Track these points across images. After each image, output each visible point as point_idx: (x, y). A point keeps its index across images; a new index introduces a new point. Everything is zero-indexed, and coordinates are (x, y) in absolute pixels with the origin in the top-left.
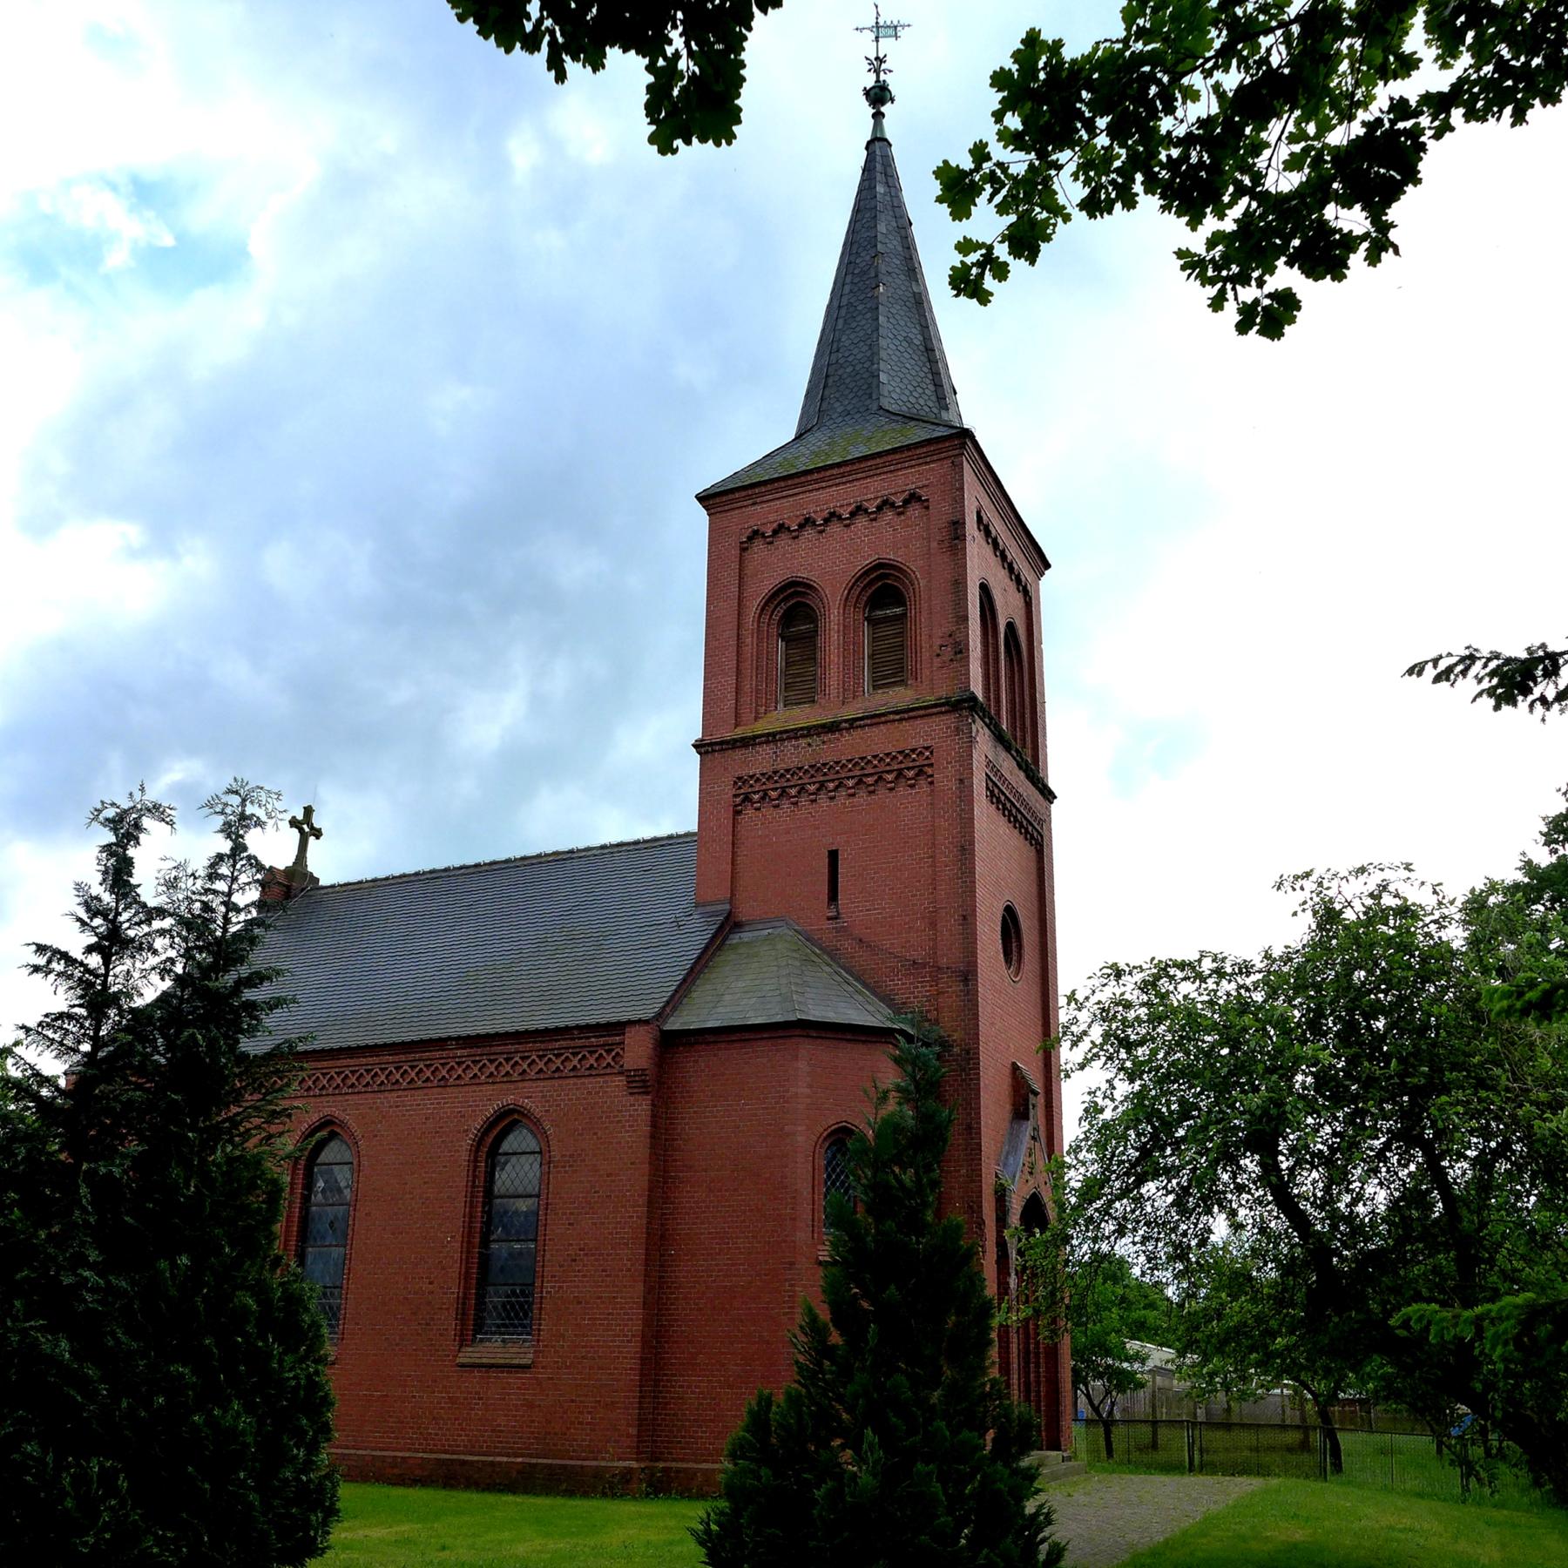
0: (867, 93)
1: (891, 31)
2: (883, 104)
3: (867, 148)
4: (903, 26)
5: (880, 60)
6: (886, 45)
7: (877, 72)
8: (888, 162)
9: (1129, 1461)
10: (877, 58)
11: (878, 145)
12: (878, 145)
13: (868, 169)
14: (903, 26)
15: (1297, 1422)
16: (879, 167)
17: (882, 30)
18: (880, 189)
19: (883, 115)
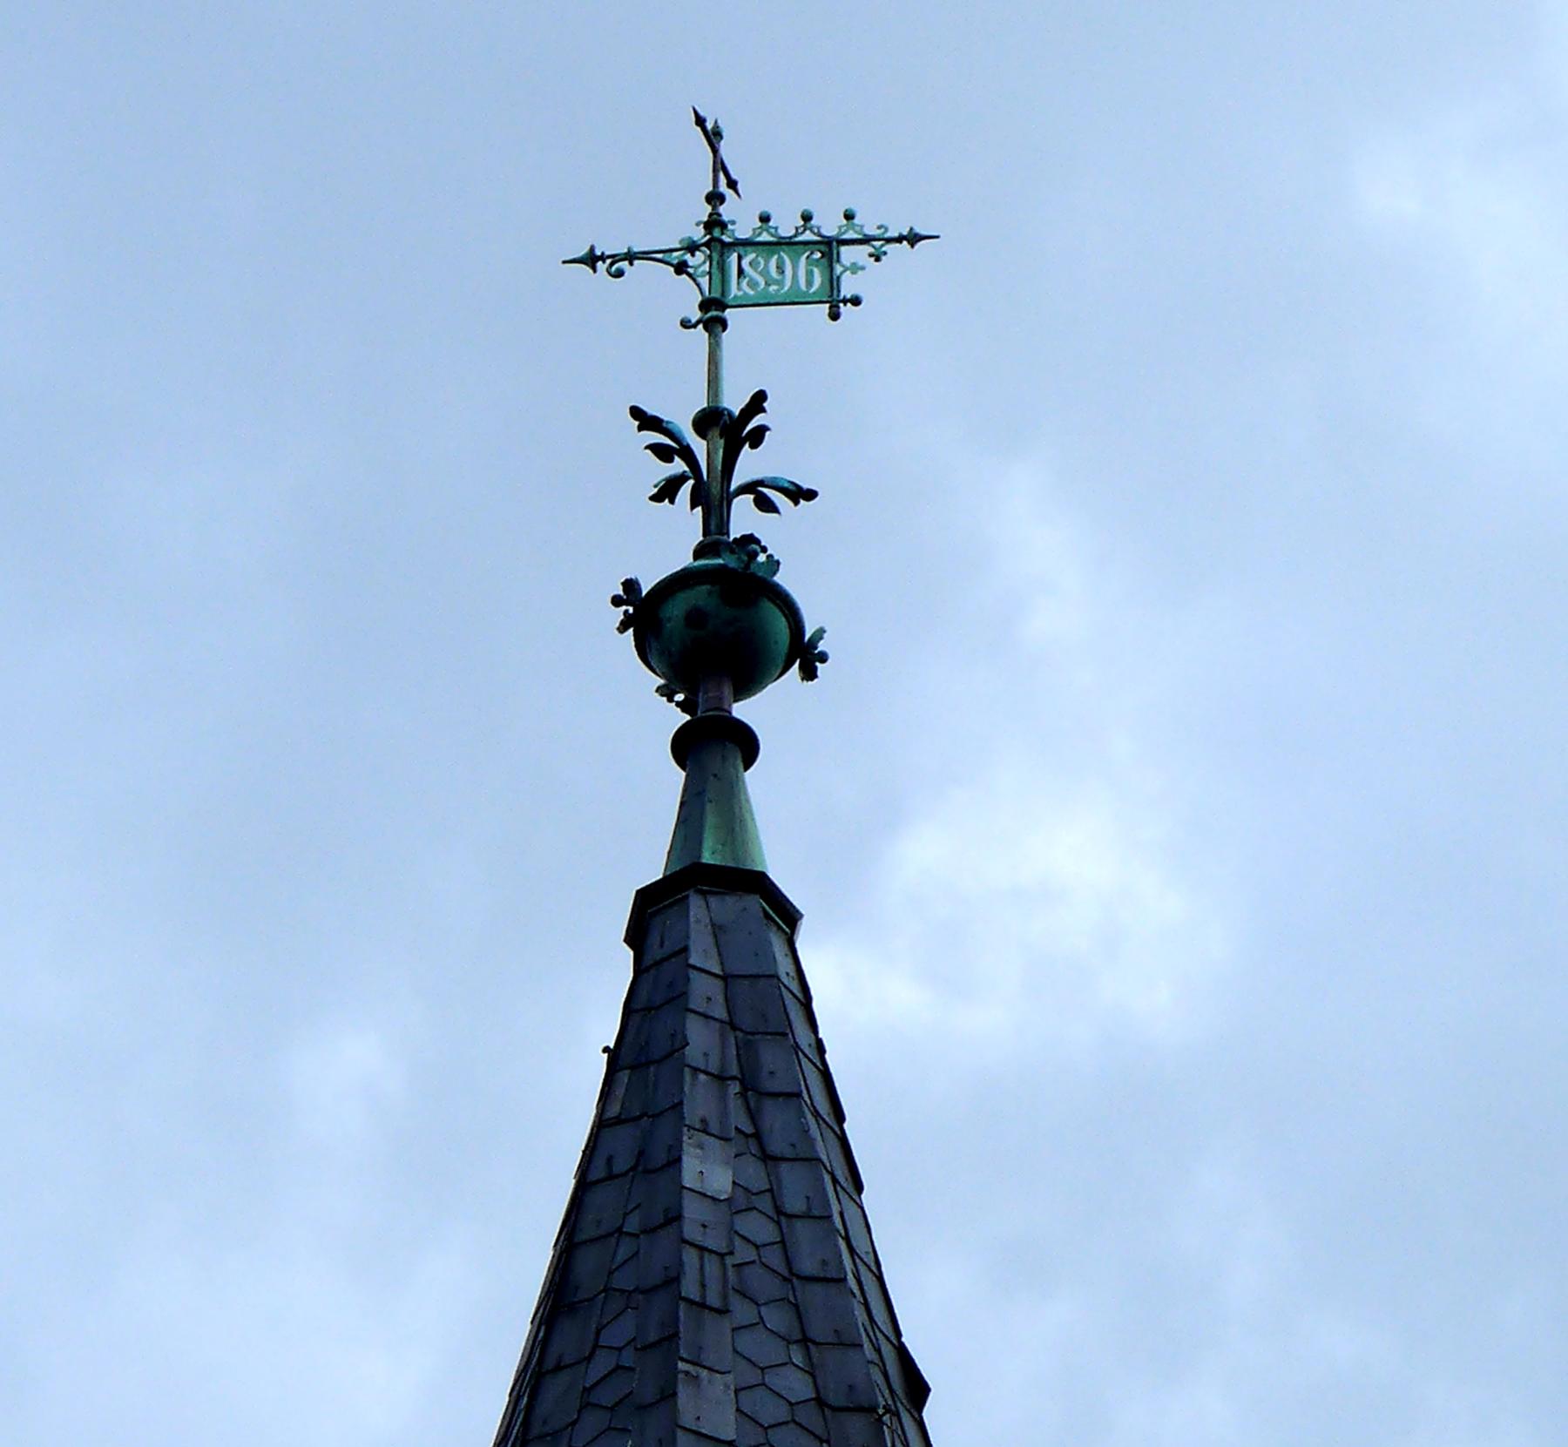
0: (645, 613)
1: (802, 272)
2: (749, 682)
3: (635, 936)
4: (877, 243)
5: (733, 428)
6: (768, 349)
7: (713, 501)
8: (774, 1018)
9: (829, 248)
10: (708, 421)
11: (712, 976)
12: (712, 976)
13: (641, 1059)
14: (877, 243)
15: (769, 1104)
16: (701, 1042)
17: (720, 262)
18: (708, 1171)
19: (746, 745)
